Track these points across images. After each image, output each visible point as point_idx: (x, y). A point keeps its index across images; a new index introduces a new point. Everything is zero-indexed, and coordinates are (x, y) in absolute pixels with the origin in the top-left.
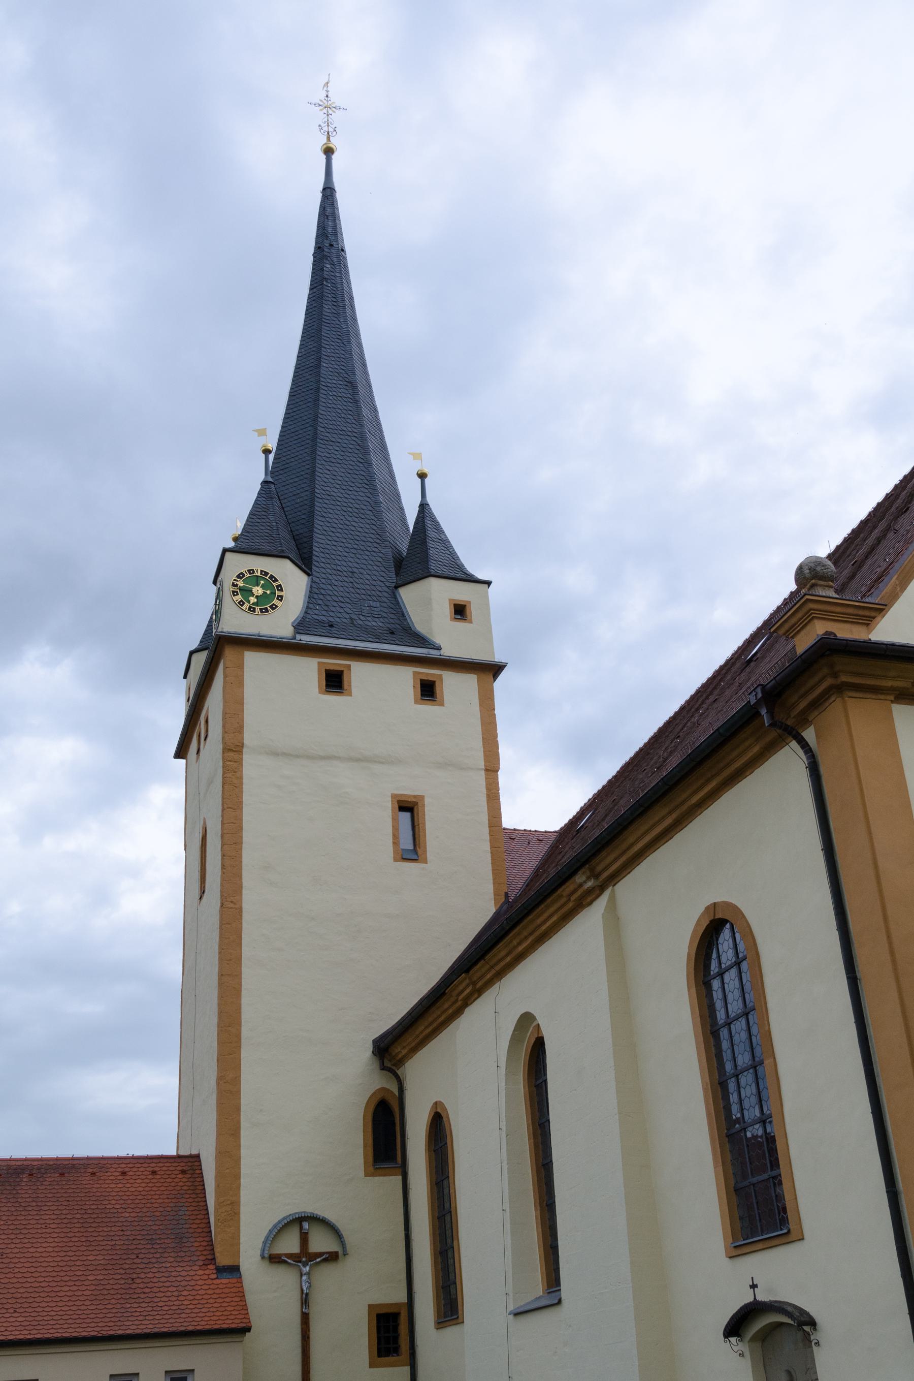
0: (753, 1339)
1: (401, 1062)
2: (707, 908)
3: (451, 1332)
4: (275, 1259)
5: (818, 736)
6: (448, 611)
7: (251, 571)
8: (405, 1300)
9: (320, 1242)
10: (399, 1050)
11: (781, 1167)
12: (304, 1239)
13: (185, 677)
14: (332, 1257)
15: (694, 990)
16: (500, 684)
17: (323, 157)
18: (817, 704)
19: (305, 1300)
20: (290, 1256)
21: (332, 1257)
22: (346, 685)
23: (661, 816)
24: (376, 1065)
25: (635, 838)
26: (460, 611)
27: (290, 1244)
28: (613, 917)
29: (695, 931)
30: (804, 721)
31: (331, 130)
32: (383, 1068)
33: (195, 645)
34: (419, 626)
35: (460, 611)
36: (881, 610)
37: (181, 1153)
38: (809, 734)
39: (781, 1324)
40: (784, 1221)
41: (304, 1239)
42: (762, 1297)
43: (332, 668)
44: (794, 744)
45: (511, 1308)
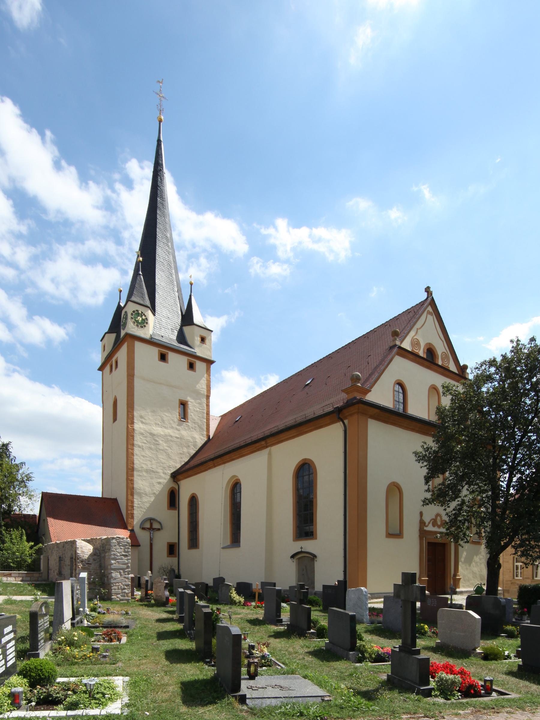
0: (297, 559)
1: (180, 480)
2: (303, 459)
3: (194, 551)
4: (143, 529)
5: (348, 423)
6: (199, 339)
7: (137, 311)
8: (177, 542)
9: (156, 526)
10: (179, 477)
11: (41, 495)
12: (151, 524)
13: (101, 341)
14: (159, 529)
15: (294, 479)
16: (213, 366)
17: (158, 123)
18: (351, 415)
19: (151, 539)
20: (148, 528)
21: (159, 529)
22: (167, 360)
23: (293, 432)
24: (172, 480)
25: (281, 436)
26: (203, 340)
27: (148, 525)
28: (270, 454)
29: (297, 464)
30: (346, 418)
31: (161, 109)
32: (174, 481)
33: (107, 330)
34: (189, 342)
35: (203, 340)
36: (368, 391)
37: (104, 496)
38: (346, 421)
39: (305, 556)
40: (313, 535)
41: (151, 524)
42: (303, 550)
43: (163, 352)
44: (341, 423)
45: (222, 547)
